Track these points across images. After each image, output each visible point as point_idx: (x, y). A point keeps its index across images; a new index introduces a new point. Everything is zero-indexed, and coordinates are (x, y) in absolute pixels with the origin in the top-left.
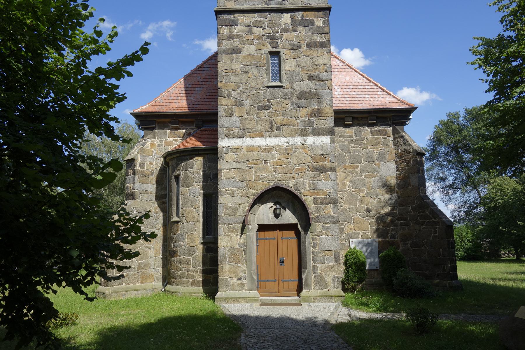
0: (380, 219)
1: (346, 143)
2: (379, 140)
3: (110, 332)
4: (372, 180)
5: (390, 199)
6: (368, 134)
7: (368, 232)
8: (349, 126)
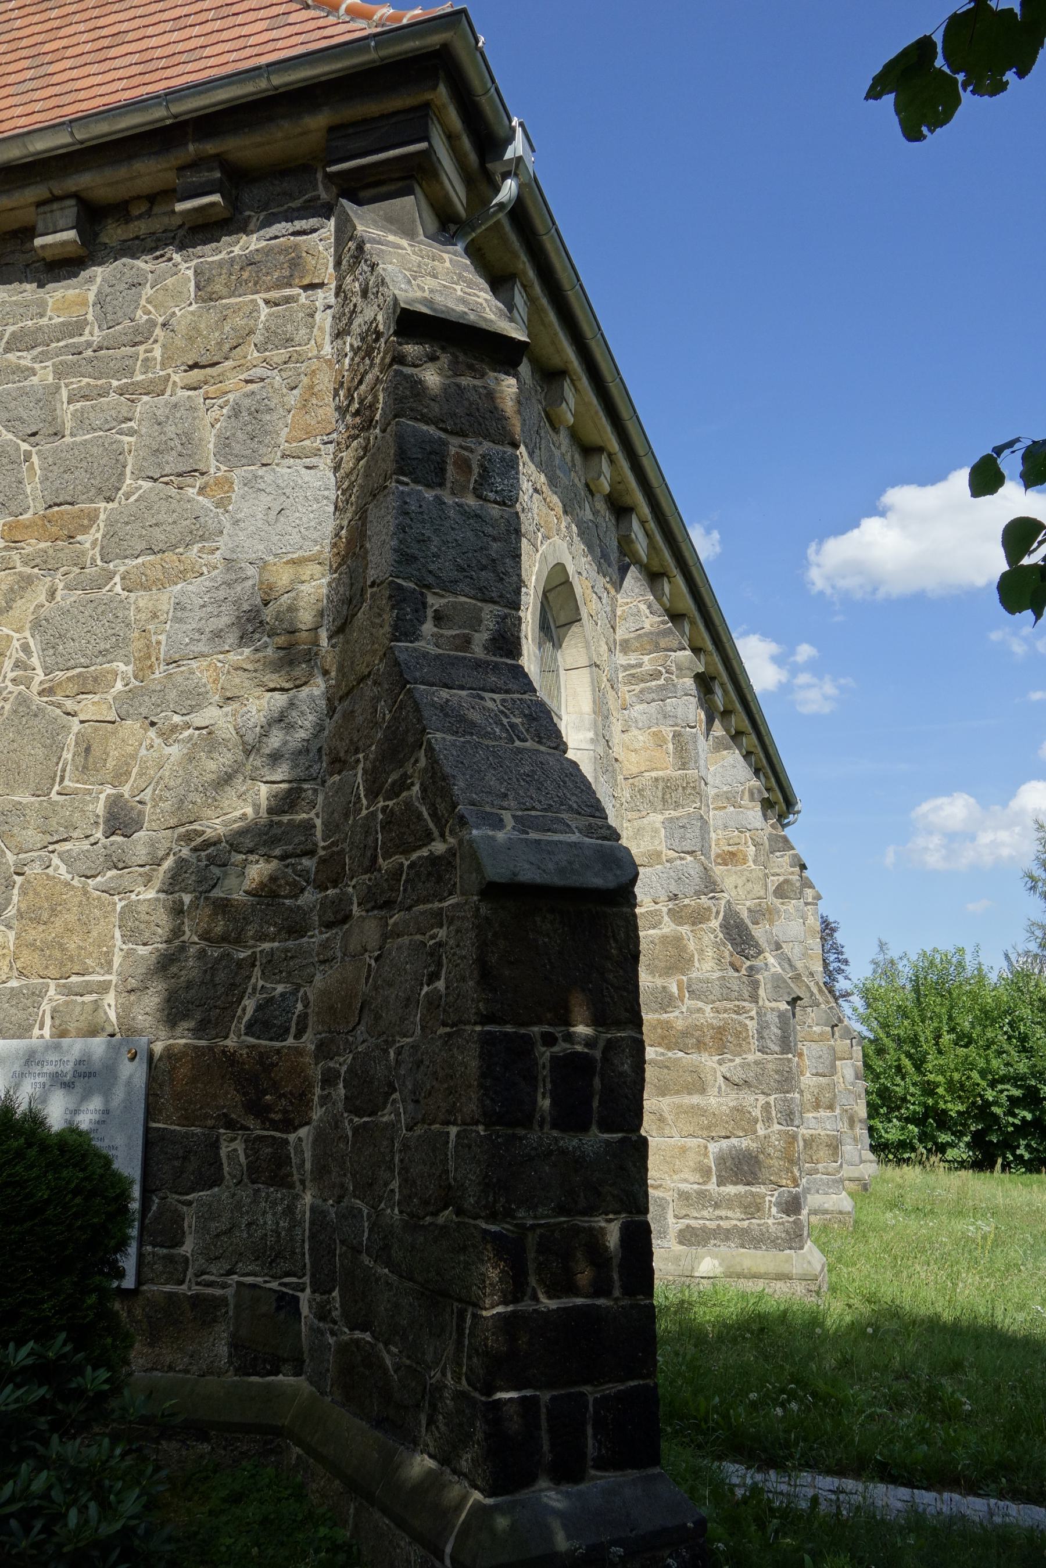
0: (200, 869)
1: (45, 375)
2: (239, 321)
3: (200, 440)
4: (165, 600)
5: (280, 719)
6: (177, 295)
7: (103, 988)
8: (62, 267)
